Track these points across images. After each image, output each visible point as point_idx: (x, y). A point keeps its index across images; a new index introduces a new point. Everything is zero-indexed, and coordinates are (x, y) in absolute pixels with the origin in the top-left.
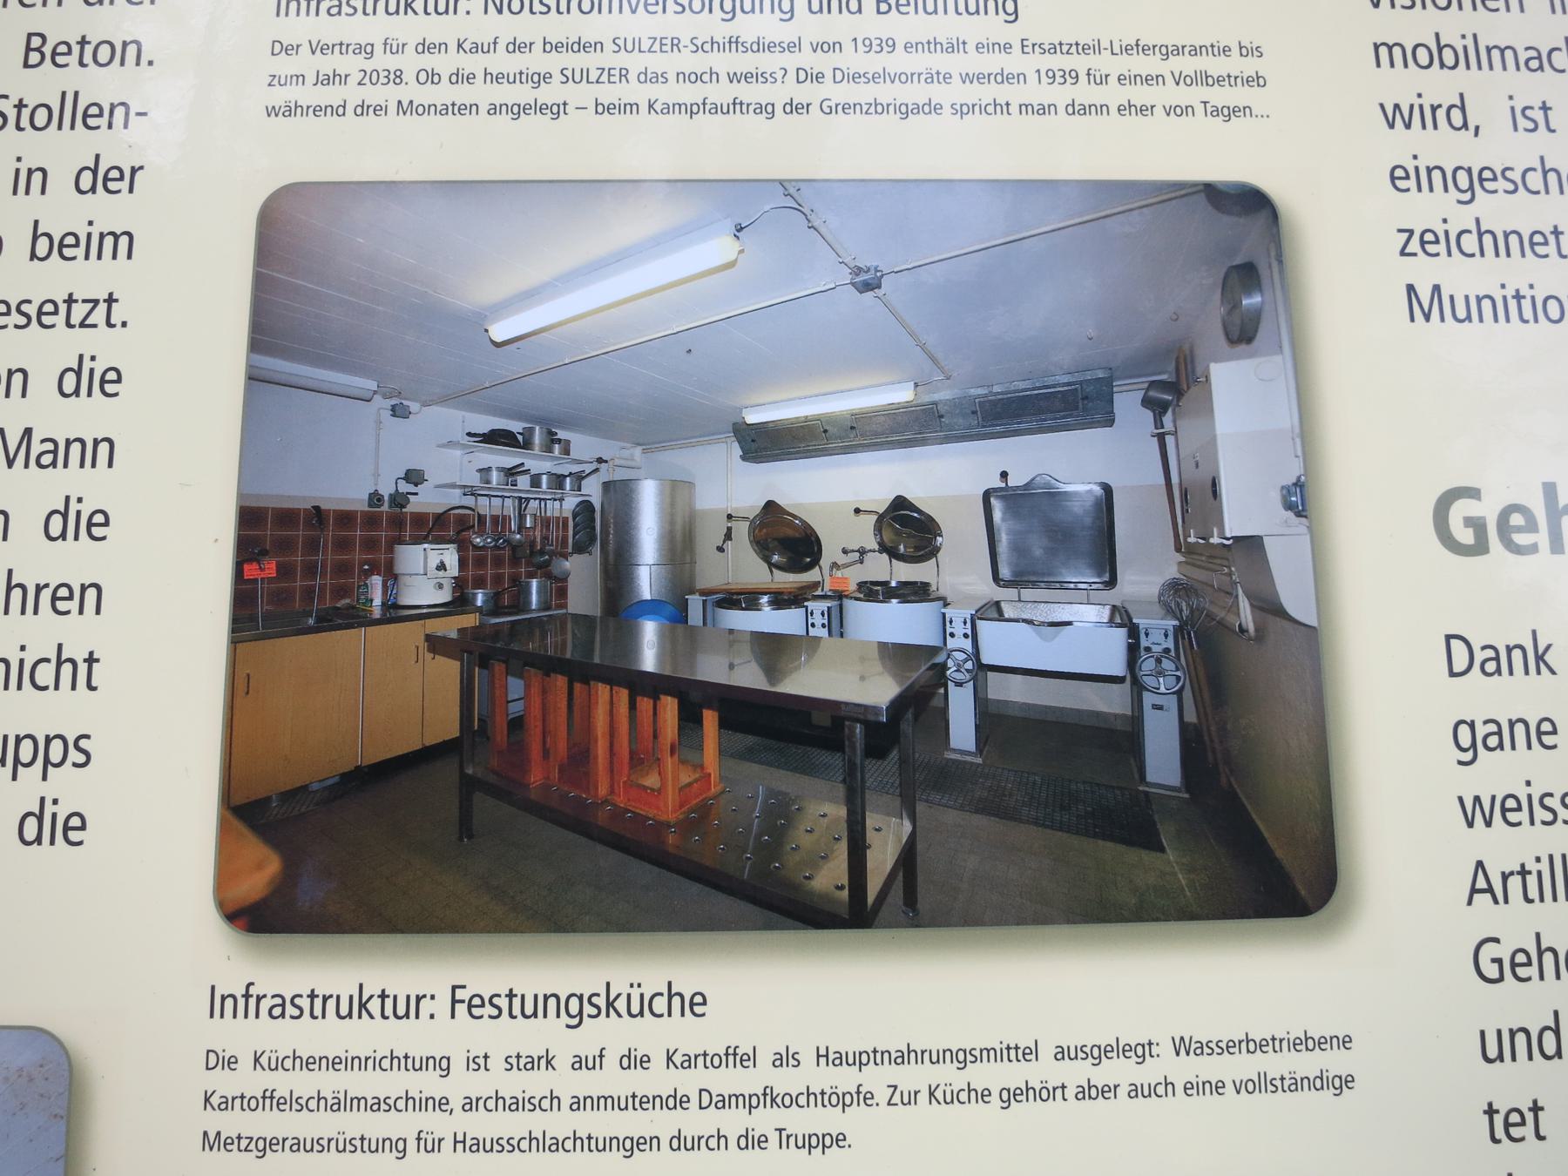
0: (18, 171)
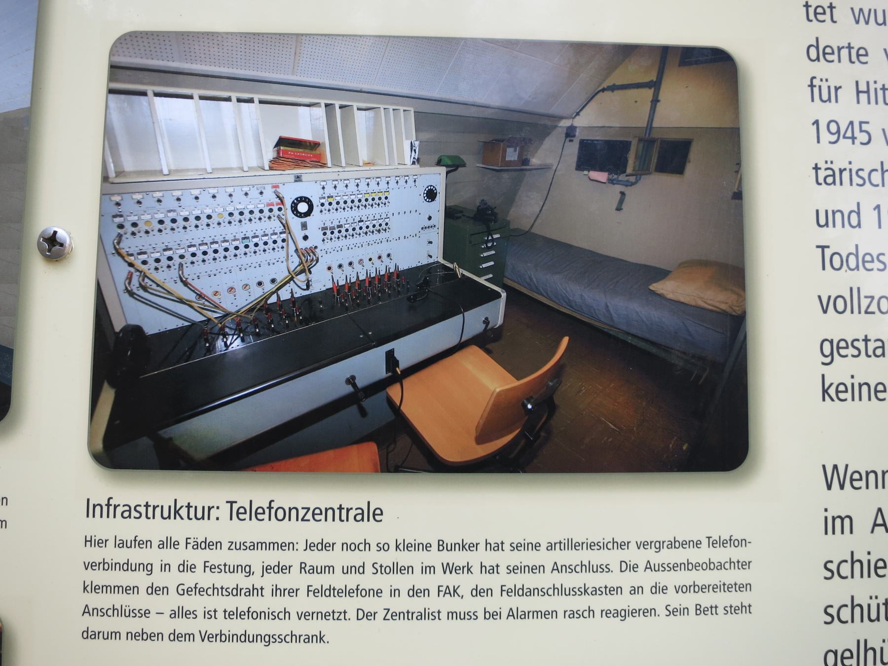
0: (162, 565)
